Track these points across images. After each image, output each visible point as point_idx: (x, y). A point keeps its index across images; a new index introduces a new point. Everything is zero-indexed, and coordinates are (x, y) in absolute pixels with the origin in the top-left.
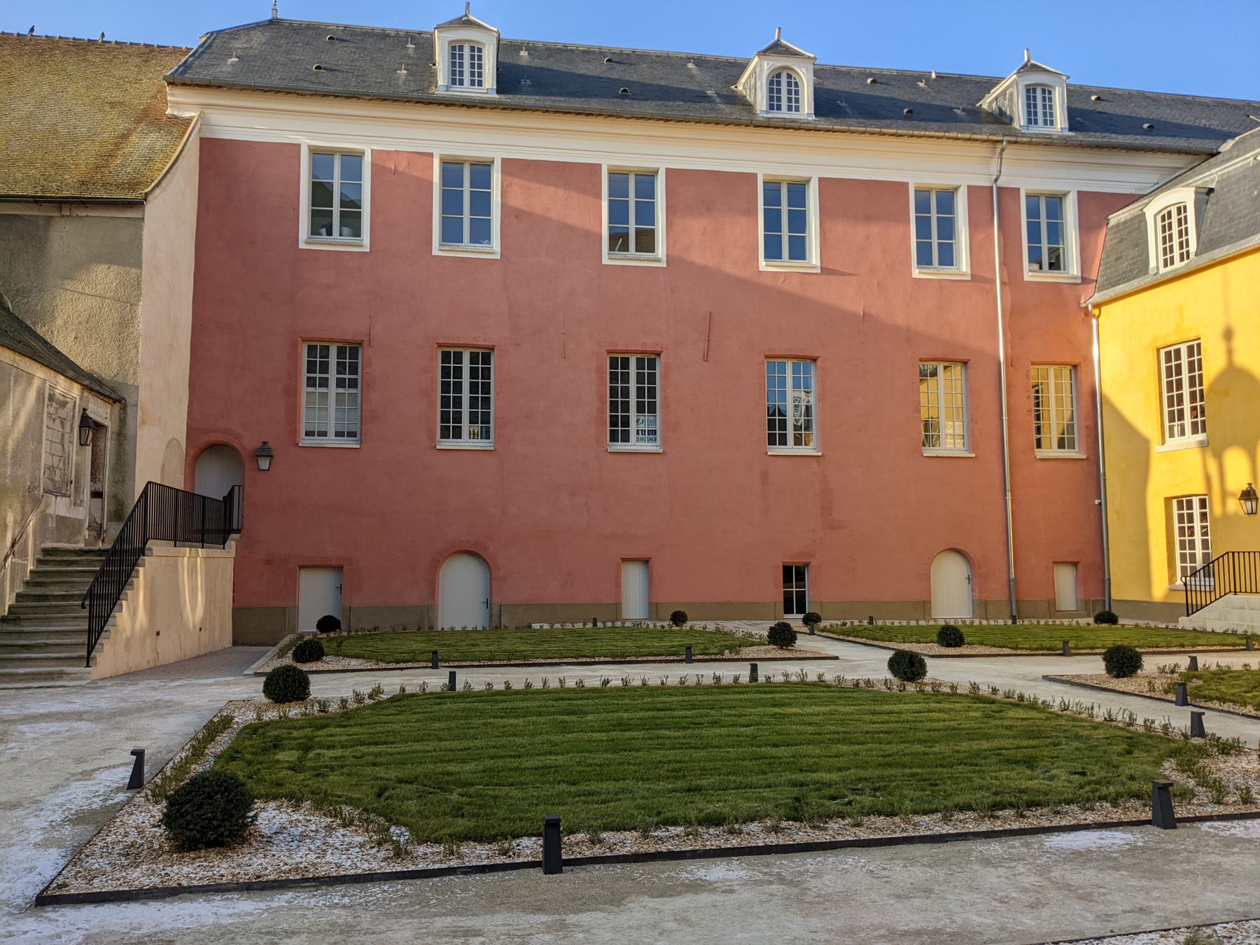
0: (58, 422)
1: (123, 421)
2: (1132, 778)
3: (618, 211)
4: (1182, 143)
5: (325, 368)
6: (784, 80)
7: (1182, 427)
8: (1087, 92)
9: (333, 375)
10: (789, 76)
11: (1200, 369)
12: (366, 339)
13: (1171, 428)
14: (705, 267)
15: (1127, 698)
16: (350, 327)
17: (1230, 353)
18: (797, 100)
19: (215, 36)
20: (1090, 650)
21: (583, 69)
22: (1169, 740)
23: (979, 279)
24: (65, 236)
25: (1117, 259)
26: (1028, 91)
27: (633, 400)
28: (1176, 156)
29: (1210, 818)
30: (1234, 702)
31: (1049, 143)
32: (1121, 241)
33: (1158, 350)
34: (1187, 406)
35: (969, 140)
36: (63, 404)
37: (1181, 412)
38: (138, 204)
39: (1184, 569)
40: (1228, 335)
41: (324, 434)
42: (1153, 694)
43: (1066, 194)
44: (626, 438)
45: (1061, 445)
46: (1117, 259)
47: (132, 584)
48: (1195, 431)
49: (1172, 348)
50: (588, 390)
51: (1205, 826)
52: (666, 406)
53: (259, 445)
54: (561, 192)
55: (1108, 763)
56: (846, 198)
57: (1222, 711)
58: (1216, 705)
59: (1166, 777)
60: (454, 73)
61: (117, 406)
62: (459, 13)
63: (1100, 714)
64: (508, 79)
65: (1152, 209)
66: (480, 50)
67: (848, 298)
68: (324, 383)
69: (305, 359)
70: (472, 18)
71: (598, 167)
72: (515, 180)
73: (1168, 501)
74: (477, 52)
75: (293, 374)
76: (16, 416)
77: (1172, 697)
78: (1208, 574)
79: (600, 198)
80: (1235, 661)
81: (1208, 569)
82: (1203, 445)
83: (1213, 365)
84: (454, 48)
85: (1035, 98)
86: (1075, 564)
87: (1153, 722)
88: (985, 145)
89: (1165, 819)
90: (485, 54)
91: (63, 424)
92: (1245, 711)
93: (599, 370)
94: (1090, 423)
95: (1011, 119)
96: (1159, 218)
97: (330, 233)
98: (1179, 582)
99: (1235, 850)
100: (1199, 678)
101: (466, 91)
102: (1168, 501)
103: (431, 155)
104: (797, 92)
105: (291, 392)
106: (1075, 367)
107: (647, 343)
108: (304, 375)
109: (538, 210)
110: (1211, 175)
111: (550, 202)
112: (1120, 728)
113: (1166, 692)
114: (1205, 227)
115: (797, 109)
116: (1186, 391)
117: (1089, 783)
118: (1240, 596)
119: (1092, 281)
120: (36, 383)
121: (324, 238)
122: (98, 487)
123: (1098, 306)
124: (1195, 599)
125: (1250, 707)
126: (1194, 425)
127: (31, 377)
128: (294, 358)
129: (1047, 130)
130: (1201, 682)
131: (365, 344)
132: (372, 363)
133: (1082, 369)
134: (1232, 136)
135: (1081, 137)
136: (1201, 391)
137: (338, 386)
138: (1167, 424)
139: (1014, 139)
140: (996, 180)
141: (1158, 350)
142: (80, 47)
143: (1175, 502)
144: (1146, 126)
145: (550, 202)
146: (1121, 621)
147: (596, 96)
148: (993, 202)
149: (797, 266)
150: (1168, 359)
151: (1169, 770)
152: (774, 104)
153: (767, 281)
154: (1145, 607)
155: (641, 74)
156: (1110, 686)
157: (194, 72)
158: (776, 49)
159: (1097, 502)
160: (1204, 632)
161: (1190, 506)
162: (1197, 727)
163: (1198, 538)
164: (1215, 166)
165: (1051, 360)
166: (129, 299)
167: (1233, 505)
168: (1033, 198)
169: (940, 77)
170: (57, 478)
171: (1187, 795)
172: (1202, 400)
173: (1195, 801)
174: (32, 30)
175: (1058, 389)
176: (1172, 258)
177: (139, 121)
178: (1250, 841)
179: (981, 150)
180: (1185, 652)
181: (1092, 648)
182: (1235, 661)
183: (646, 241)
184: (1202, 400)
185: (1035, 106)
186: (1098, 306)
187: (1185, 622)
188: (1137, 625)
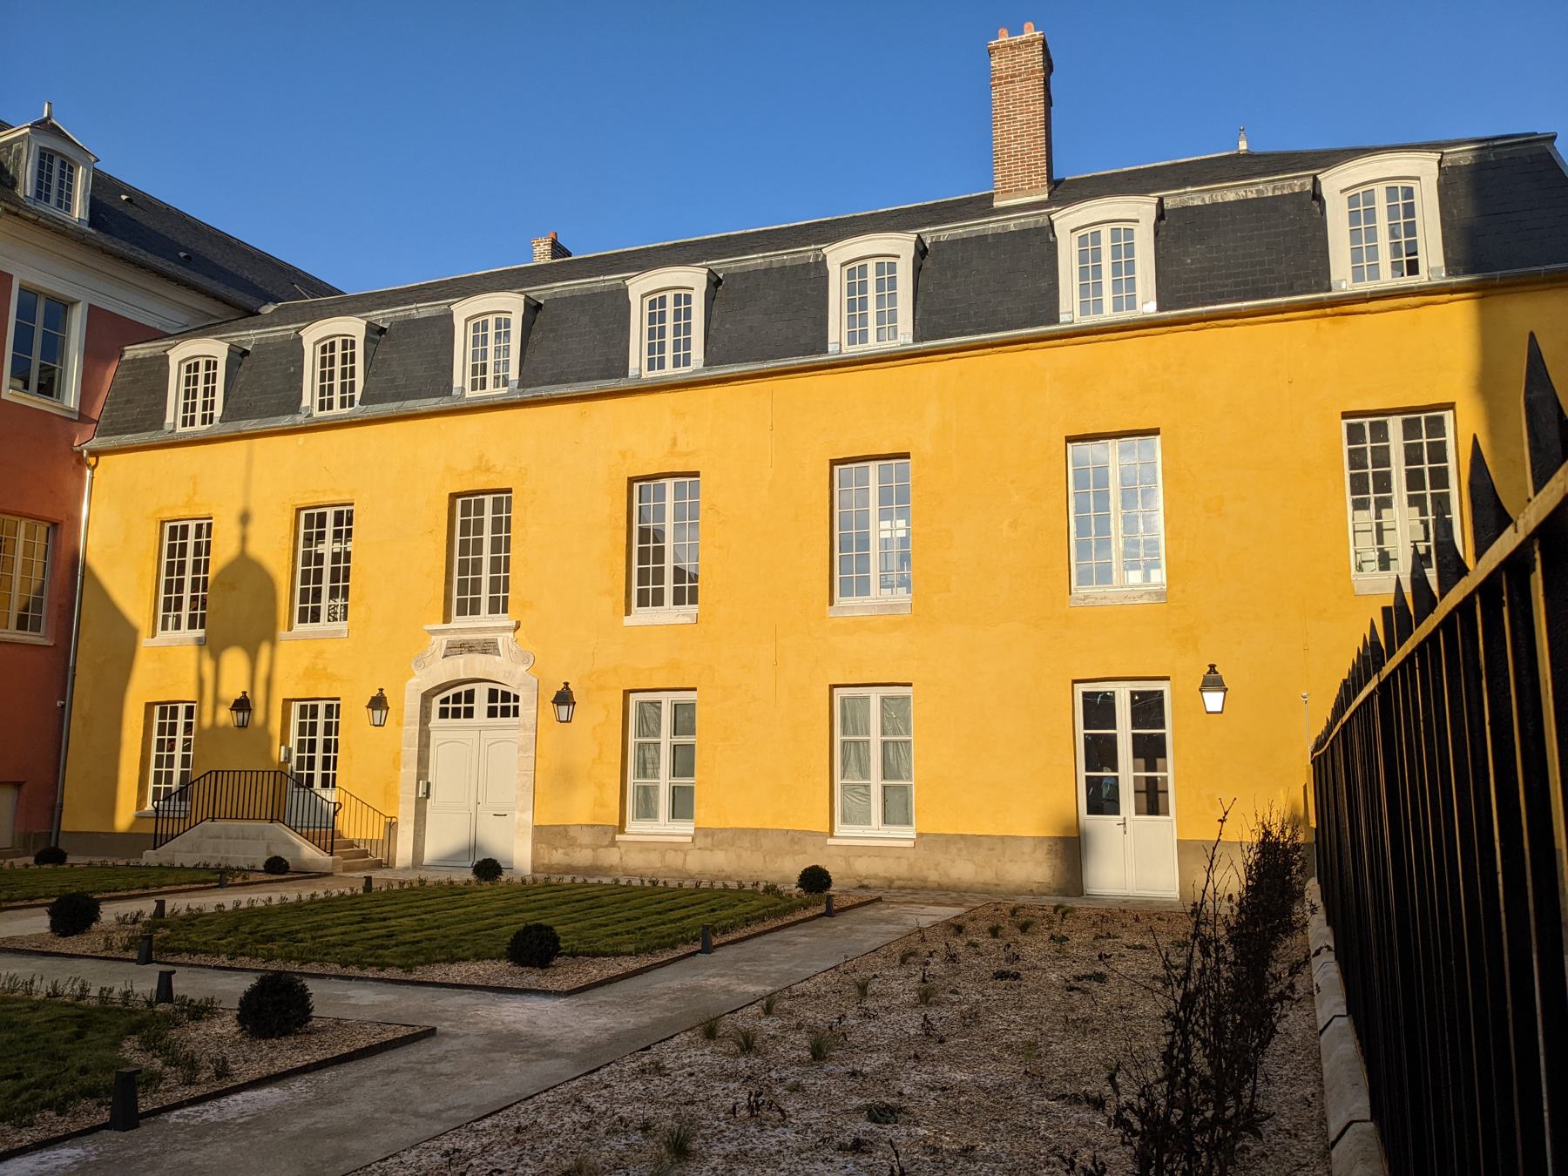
2: (84, 1071)
7: (178, 619)
8: (120, 187)
11: (208, 553)
13: (165, 619)
15: (77, 962)
17: (244, 539)
20: (29, 902)
22: (130, 1012)
25: (128, 401)
26: (42, 155)
28: (212, 301)
29: (180, 1105)
30: (206, 952)
31: (61, 231)
32: (135, 382)
33: (163, 523)
34: (187, 594)
37: (179, 601)
39: (156, 791)
40: (245, 519)
42: (109, 953)
43: (74, 303)
45: (22, 624)
46: (128, 401)
48: (192, 626)
49: (179, 524)
51: (173, 1117)
55: (52, 1056)
57: (192, 965)
58: (186, 958)
59: (127, 1063)
63: (42, 988)
65: (180, 353)
73: (149, 707)
77: (133, 954)
78: (182, 800)
80: (207, 902)
81: (183, 793)
82: (201, 643)
83: (223, 551)
85: (50, 169)
86: (18, 785)
87: (111, 991)
89: (127, 1118)
92: (218, 962)
96: (319, 348)
98: (149, 807)
99: (209, 1139)
100: (165, 926)
102: (149, 707)
106: (55, 525)
110: (250, 337)
112: (67, 1005)
113: (126, 949)
116: (188, 576)
117: (27, 1088)
119: (92, 421)
123: (96, 454)
124: (164, 828)
125: (223, 957)
126: (192, 618)
129: (60, 214)
130: (168, 932)
135: (103, 239)
136: (206, 579)
139: (15, 209)
141: (163, 523)
143: (157, 708)
144: (182, 254)
146: (70, 860)
150: (173, 536)
151: (132, 1052)
154: (110, 841)
156: (54, 949)
159: (59, 704)
160: (171, 868)
161: (174, 715)
162: (165, 989)
163: (178, 753)
164: (254, 327)
167: (225, 716)
171: (154, 1079)
172: (204, 589)
173: (161, 1087)
176: (193, 418)
178: (225, 1124)
180: (148, 895)
181: (31, 899)
182: (207, 902)
184: (204, 589)
185: (49, 178)
186: (96, 454)
187: (150, 857)
188: (90, 864)
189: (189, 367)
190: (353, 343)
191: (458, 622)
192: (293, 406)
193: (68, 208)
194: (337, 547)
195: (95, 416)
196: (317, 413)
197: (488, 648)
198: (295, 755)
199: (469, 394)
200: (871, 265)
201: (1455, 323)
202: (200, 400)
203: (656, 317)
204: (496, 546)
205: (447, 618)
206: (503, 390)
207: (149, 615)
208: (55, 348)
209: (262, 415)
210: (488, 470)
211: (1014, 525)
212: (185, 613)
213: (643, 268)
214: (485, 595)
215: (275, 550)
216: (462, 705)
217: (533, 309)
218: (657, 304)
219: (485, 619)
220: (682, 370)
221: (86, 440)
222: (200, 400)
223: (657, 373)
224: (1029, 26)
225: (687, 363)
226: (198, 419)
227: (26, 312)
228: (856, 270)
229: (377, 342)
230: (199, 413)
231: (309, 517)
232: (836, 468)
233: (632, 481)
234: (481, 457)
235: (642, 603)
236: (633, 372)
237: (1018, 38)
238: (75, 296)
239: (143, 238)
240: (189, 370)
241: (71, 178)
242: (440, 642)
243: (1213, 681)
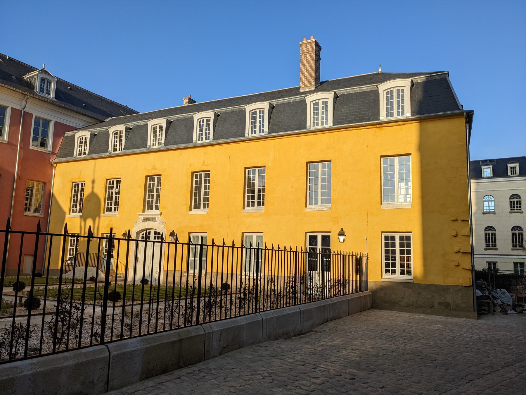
4: (93, 115)
13: (73, 210)
17: (93, 188)
23: (11, 144)
25: (65, 148)
31: (46, 101)
34: (78, 203)
40: (93, 182)
43: (51, 121)
46: (65, 148)
48: (79, 212)
65: (79, 134)
82: (81, 217)
83: (87, 191)
85: (44, 83)
95: (34, 88)
96: (199, 121)
106: (45, 183)
110: (97, 130)
114: (92, 146)
116: (79, 198)
119: (55, 154)
123: (56, 163)
129: (47, 96)
133: (48, 184)
134: (111, 116)
135: (59, 103)
138: (72, 208)
140: (24, 109)
169: (10, 59)
175: (37, 190)
176: (202, 138)
179: (21, 96)
185: (44, 86)
186: (56, 163)
189: (200, 121)
190: (210, 120)
191: (148, 212)
192: (106, 150)
193: (49, 94)
194: (117, 190)
195: (56, 153)
196: (113, 152)
197: (153, 220)
198: (104, 249)
200: (395, 90)
201: (414, 128)
202: (118, 143)
203: (254, 118)
204: (205, 188)
206: (160, 146)
207: (68, 209)
208: (45, 134)
209: (98, 153)
210: (155, 169)
211: (292, 187)
212: (78, 208)
213: (249, 103)
214: (202, 203)
215: (100, 191)
216: (157, 236)
217: (169, 123)
218: (254, 113)
219: (154, 211)
220: (207, 141)
221: (54, 159)
222: (118, 143)
223: (201, 142)
224: (312, 37)
225: (209, 139)
226: (118, 149)
227: (37, 123)
228: (254, 113)
229: (129, 132)
230: (83, 152)
231: (110, 182)
232: (382, 158)
233: (246, 168)
235: (195, 208)
236: (194, 142)
237: (308, 41)
238: (51, 119)
239: (73, 100)
240: (200, 123)
241: (50, 85)
242: (141, 218)
243: (342, 233)
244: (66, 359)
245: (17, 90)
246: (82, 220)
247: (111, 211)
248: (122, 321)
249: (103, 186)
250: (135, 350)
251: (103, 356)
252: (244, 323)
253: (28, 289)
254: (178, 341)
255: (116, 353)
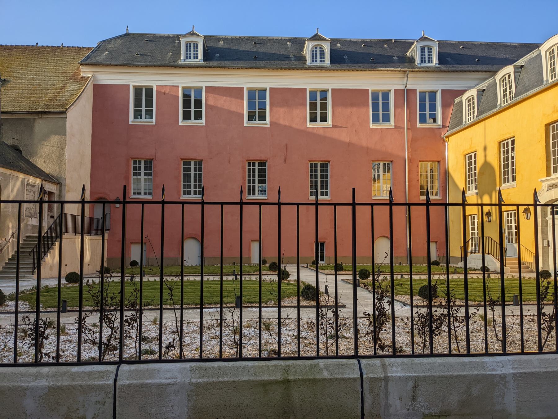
0: (32, 192)
1: (60, 191)
3: (251, 104)
5: (140, 169)
6: (318, 50)
9: (143, 171)
10: (320, 48)
12: (154, 158)
14: (285, 126)
16: (149, 153)
17: (485, 156)
18: (324, 58)
19: (102, 42)
21: (245, 47)
24: (40, 125)
26: (422, 49)
27: (257, 179)
28: (485, 73)
31: (428, 71)
33: (465, 155)
35: (393, 71)
36: (34, 186)
38: (64, 113)
40: (485, 149)
41: (139, 193)
44: (254, 194)
47: (53, 248)
49: (470, 155)
50: (238, 177)
52: (269, 181)
53: (116, 198)
54: (228, 98)
56: (341, 95)
60: (187, 54)
61: (58, 185)
62: (190, 30)
64: (208, 56)
65: (465, 97)
66: (197, 45)
67: (344, 136)
68: (140, 174)
69: (132, 166)
70: (195, 32)
71: (242, 88)
72: (210, 95)
74: (196, 45)
75: (128, 172)
76: (12, 191)
79: (243, 100)
82: (477, 194)
83: (480, 161)
84: (187, 44)
88: (400, 73)
90: (199, 46)
91: (34, 193)
93: (243, 168)
94: (443, 185)
97: (141, 118)
101: (192, 61)
103: (178, 86)
104: (324, 55)
105: (127, 178)
106: (439, 162)
107: (263, 157)
108: (132, 172)
109: (219, 106)
110: (484, 85)
111: (223, 102)
115: (324, 61)
118: (476, 254)
119: (446, 127)
120: (21, 179)
121: (139, 120)
122: (52, 214)
123: (447, 137)
127: (18, 178)
128: (128, 165)
129: (430, 65)
131: (154, 159)
132: (157, 166)
133: (442, 163)
135: (442, 67)
137: (145, 175)
141: (465, 155)
142: (54, 49)
145: (223, 102)
147: (243, 60)
148: (405, 96)
149: (324, 124)
152: (314, 60)
153: (310, 130)
155: (268, 49)
157: (94, 57)
158: (316, 37)
165: (428, 159)
166: (62, 147)
168: (422, 94)
169: (396, 41)
170: (32, 212)
174: (37, 44)
177: (70, 79)
179: (400, 75)
183: (263, 117)
186: (447, 137)
199: (550, 81)
205: (548, 174)
215: (493, 159)
227: (422, 99)
229: (520, 72)
234: (555, 106)
242: (545, 185)
244: (38, 376)
245: (394, 69)
246: (479, 198)
247: (508, 182)
248: (356, 331)
249: (496, 151)
250: (168, 384)
251: (101, 383)
252: (508, 370)
253: (371, 278)
254: (277, 382)
255: (128, 382)
